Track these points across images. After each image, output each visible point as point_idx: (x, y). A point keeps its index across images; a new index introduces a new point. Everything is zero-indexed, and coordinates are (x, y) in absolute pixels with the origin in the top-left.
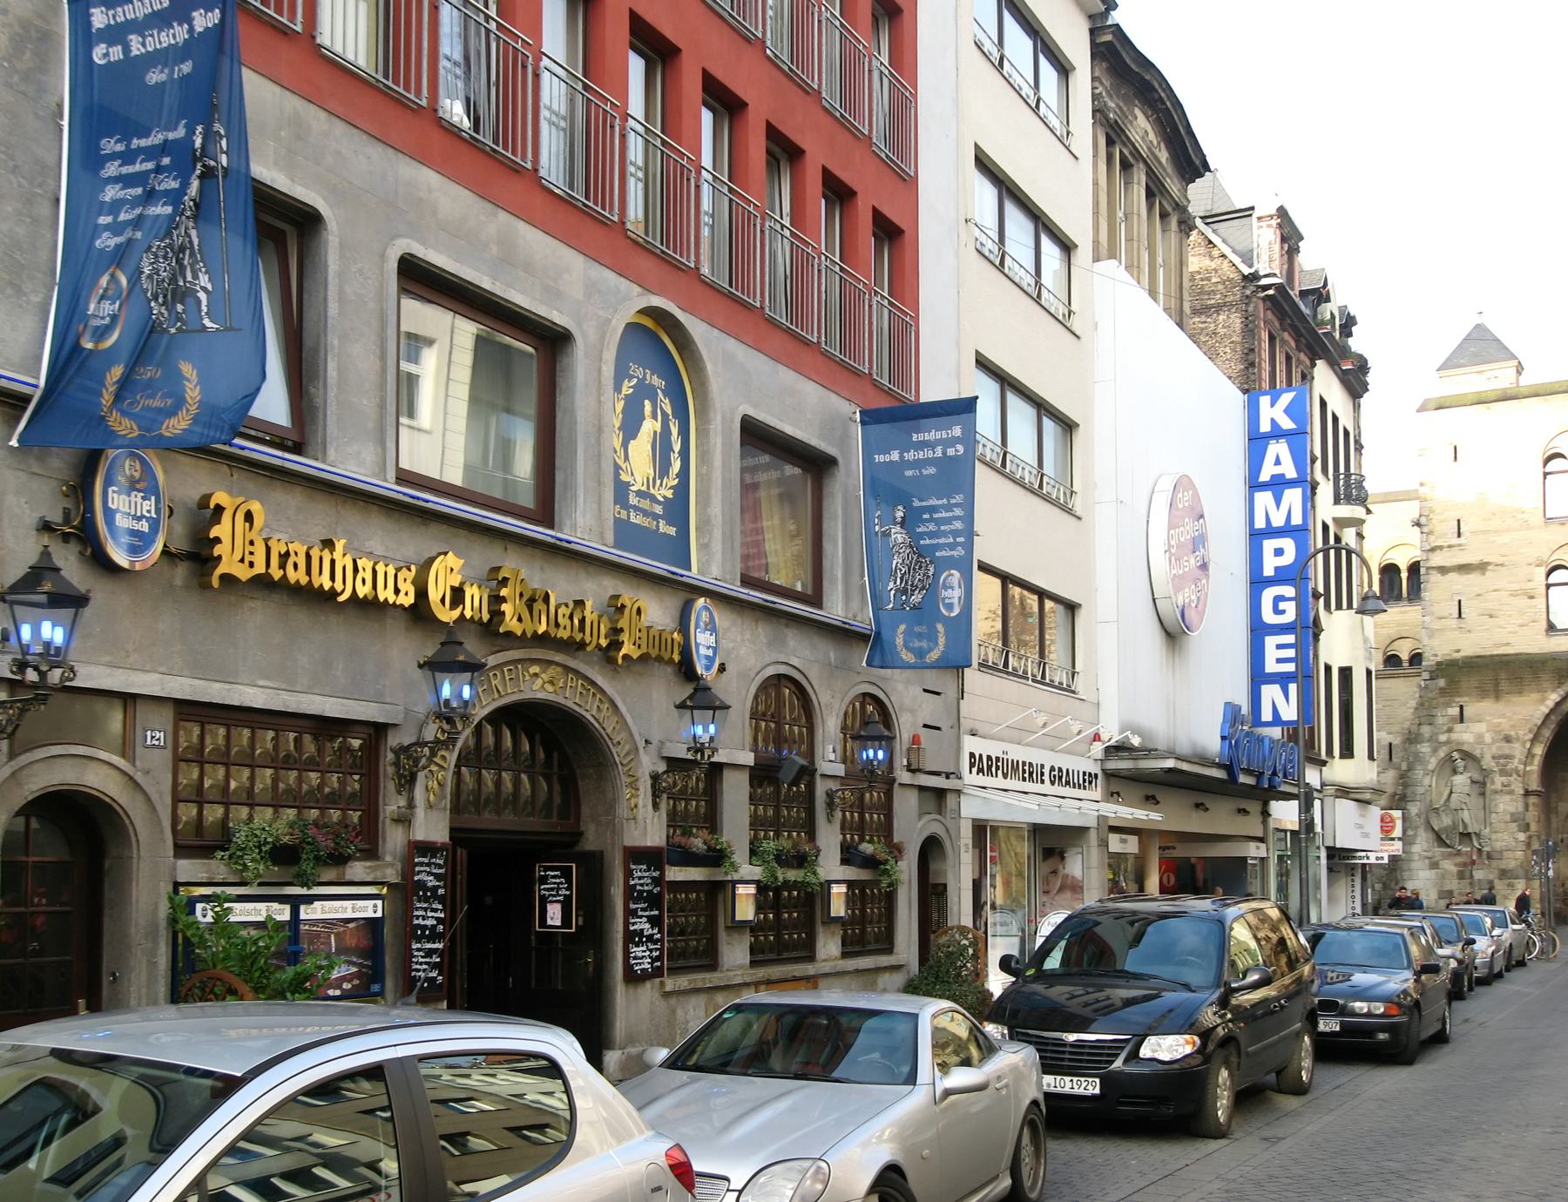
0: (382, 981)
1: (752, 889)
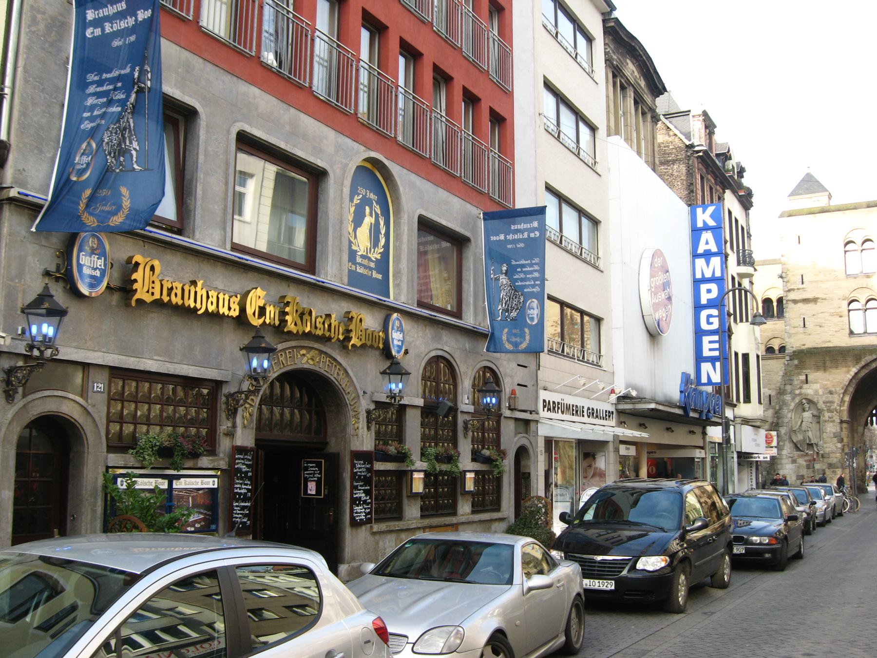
0: (217, 523)
1: (422, 475)
